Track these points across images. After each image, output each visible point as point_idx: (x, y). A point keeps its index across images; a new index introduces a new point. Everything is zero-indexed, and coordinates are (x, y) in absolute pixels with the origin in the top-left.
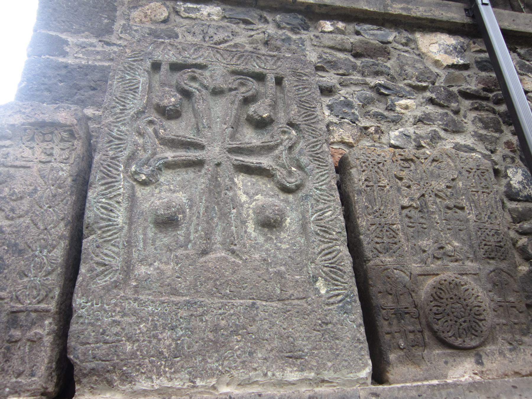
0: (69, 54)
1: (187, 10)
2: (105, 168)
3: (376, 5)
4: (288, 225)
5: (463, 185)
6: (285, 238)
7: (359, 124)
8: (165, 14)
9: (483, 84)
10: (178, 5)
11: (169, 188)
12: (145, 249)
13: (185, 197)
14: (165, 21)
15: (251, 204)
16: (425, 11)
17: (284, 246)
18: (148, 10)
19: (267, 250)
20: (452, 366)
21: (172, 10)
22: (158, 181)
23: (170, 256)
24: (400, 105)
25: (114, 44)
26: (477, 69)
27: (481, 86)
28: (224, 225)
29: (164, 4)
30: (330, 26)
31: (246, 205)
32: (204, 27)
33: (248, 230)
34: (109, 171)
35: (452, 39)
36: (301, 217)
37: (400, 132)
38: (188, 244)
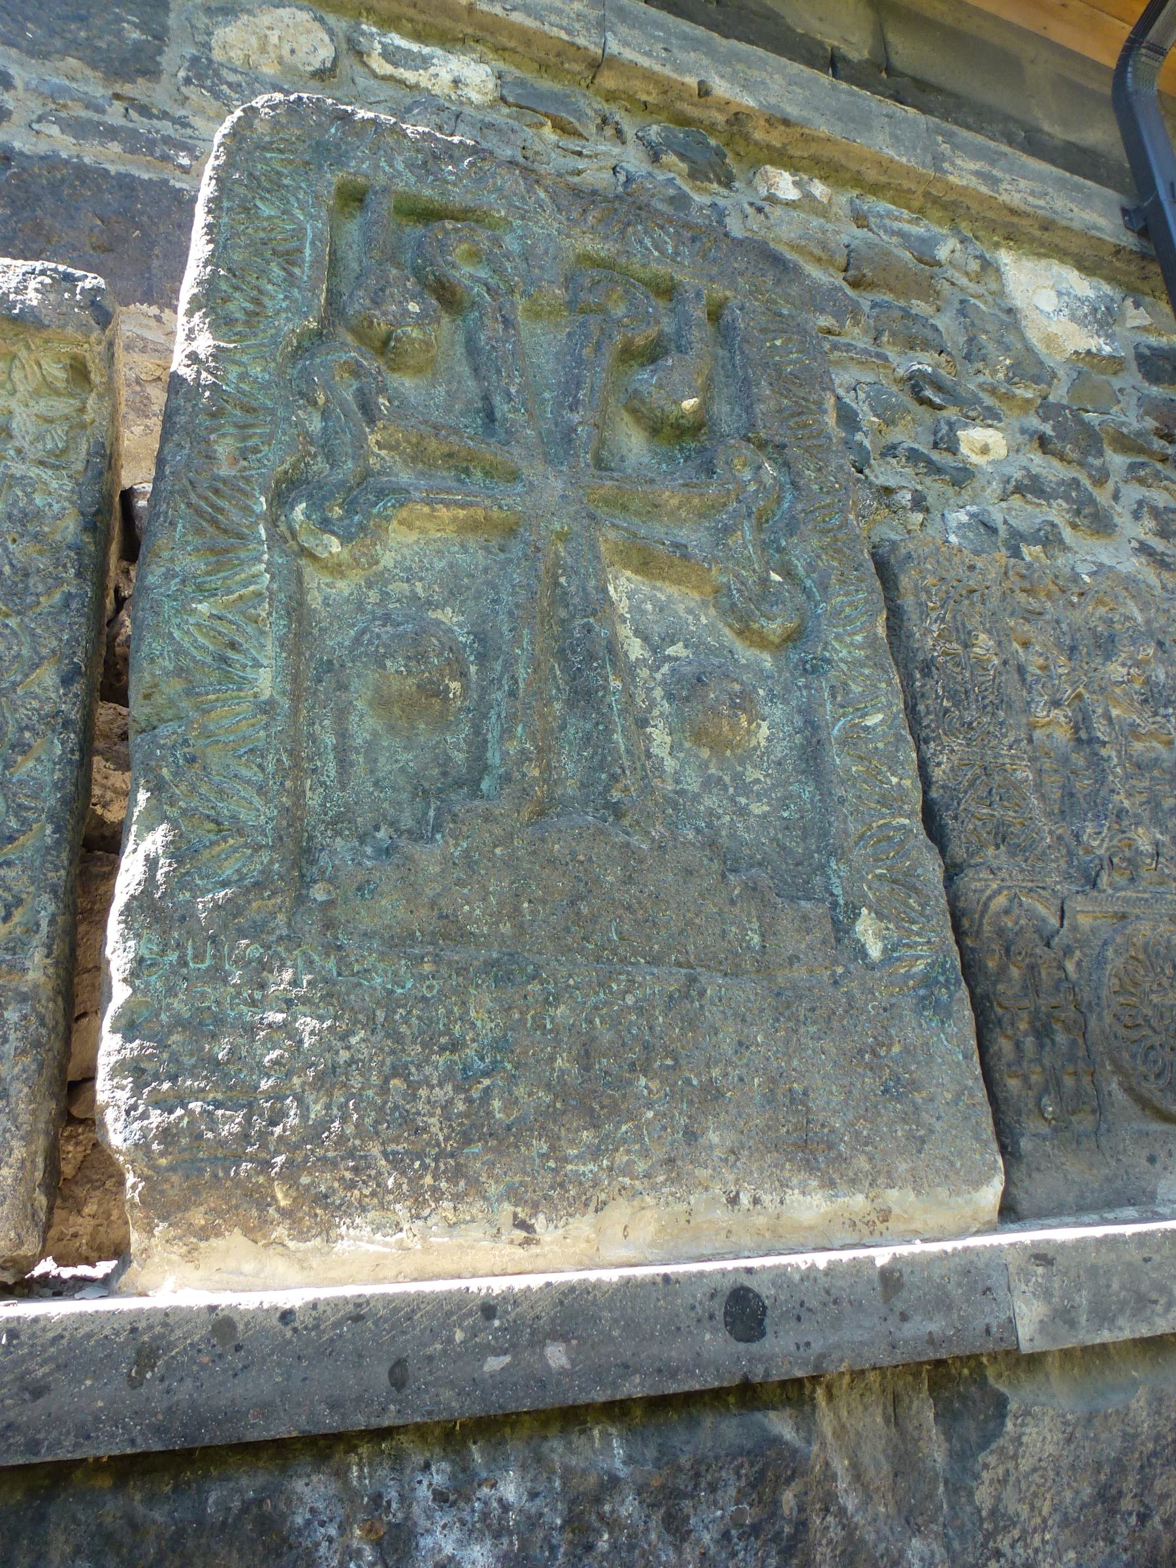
0: (15, 117)
1: (389, 55)
2: (206, 499)
3: (914, 149)
4: (763, 743)
5: (1167, 676)
6: (757, 781)
7: (872, 478)
8: (326, 53)
9: (1156, 419)
10: (363, 34)
11: (412, 591)
12: (343, 788)
13: (460, 625)
14: (322, 75)
15: (658, 668)
16: (1032, 193)
17: (758, 809)
18: (271, 28)
19: (711, 813)
20: (1165, 1168)
21: (345, 46)
22: (377, 563)
23: (425, 814)
24: (971, 442)
25: (165, 115)
26: (1140, 376)
27: (1150, 423)
28: (588, 726)
29: (321, 20)
30: (791, 186)
31: (644, 673)
32: (445, 115)
33: (654, 750)
34: (220, 510)
35: (1086, 283)
36: (798, 721)
37: (972, 515)
38: (481, 778)
